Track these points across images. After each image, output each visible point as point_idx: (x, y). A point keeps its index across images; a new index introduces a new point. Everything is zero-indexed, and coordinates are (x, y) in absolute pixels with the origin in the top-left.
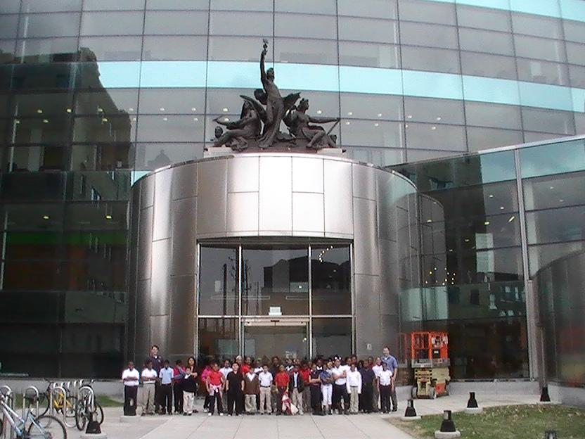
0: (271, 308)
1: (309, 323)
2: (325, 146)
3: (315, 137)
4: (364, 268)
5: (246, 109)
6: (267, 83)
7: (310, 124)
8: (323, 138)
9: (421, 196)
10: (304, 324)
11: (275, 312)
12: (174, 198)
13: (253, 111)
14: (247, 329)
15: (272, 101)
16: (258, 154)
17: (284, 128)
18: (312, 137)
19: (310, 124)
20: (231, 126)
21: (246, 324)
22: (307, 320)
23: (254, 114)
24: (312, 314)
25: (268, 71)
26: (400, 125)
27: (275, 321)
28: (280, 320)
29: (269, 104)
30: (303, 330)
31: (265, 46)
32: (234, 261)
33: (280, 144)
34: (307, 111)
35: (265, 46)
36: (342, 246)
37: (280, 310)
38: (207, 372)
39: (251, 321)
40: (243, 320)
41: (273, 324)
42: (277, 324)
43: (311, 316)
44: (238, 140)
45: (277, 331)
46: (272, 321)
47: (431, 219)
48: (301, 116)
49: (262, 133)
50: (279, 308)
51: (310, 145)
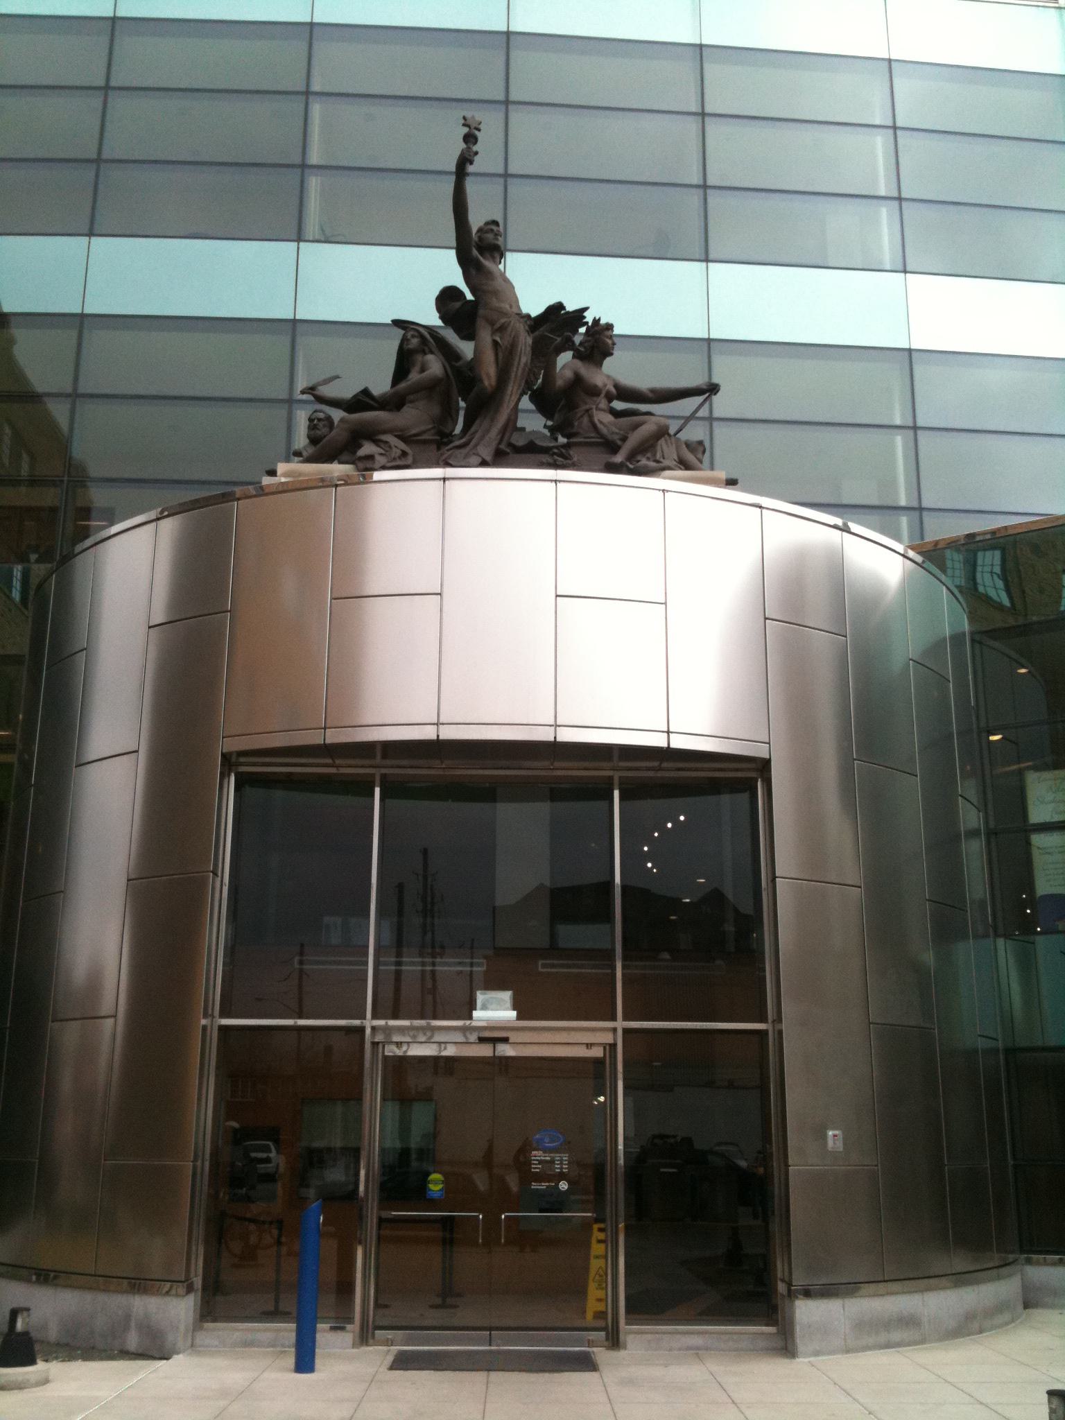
0: (481, 997)
1: (613, 1046)
2: (666, 463)
3: (634, 439)
4: (808, 858)
5: (412, 352)
6: (479, 267)
7: (619, 405)
8: (662, 442)
9: (980, 643)
10: (597, 1052)
11: (495, 1010)
12: (158, 618)
13: (430, 357)
14: (400, 1067)
15: (492, 323)
16: (438, 472)
17: (533, 422)
18: (624, 439)
19: (619, 405)
20: (363, 401)
21: (391, 1051)
22: (608, 1038)
23: (435, 366)
24: (374, 1017)
25: (480, 230)
26: (899, 440)
27: (495, 1041)
28: (514, 1037)
29: (486, 335)
30: (594, 1072)
31: (470, 139)
32: (420, 878)
33: (514, 451)
34: (608, 361)
35: (470, 139)
36: (714, 787)
37: (509, 1004)
38: (290, 1199)
39: (425, 1040)
40: (379, 1038)
41: (485, 1051)
42: (506, 1050)
43: (620, 1024)
44: (377, 442)
45: (495, 1072)
46: (482, 1040)
47: (990, 742)
48: (585, 371)
49: (458, 429)
50: (506, 996)
51: (618, 459)
